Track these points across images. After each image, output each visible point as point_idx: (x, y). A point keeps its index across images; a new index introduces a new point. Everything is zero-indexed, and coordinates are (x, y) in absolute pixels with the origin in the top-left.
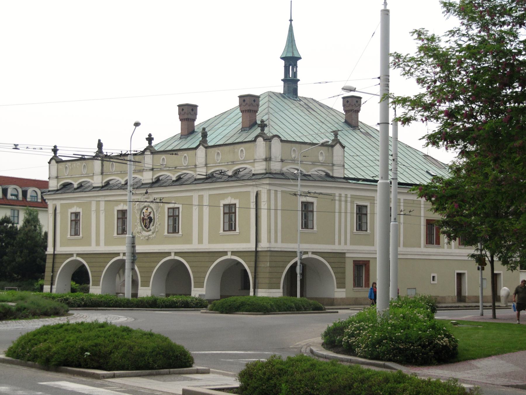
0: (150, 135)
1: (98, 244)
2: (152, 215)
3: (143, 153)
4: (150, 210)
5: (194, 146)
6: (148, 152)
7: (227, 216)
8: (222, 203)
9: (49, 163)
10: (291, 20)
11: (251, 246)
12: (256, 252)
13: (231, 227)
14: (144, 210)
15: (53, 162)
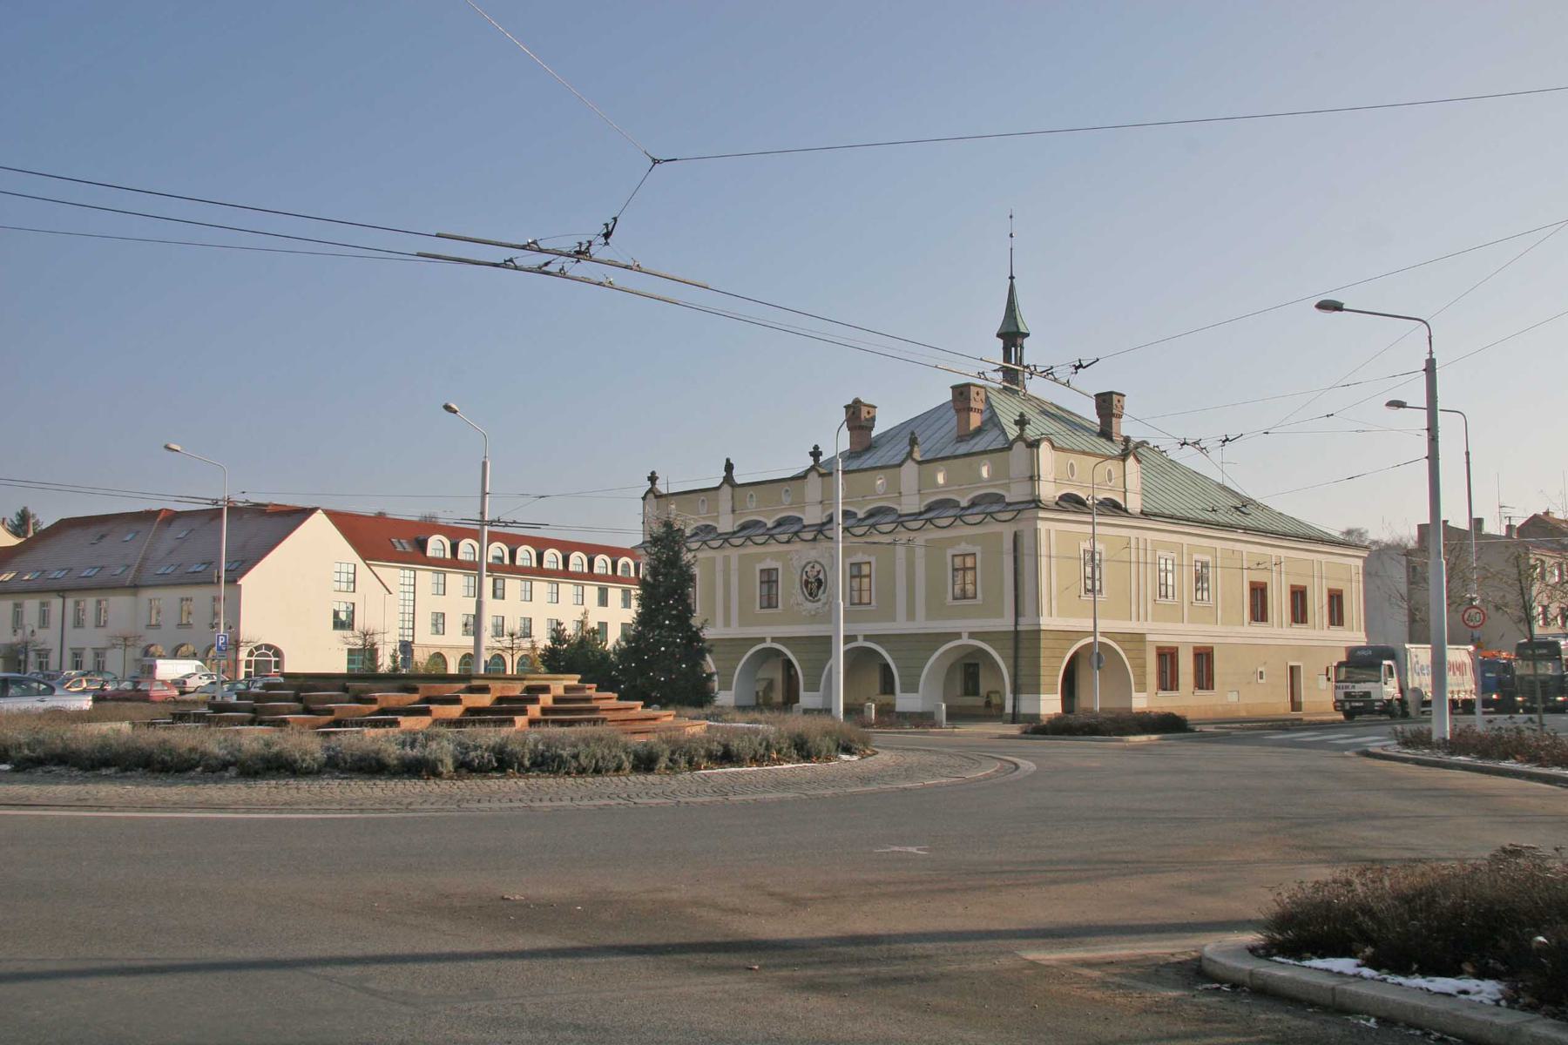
0: (816, 447)
1: (911, 615)
2: (821, 576)
3: (802, 477)
4: (818, 567)
5: (896, 461)
6: (813, 476)
7: (765, 587)
8: (759, 567)
9: (644, 498)
10: (1012, 278)
11: (1006, 623)
12: (1016, 632)
13: (770, 602)
14: (808, 569)
15: (651, 496)
